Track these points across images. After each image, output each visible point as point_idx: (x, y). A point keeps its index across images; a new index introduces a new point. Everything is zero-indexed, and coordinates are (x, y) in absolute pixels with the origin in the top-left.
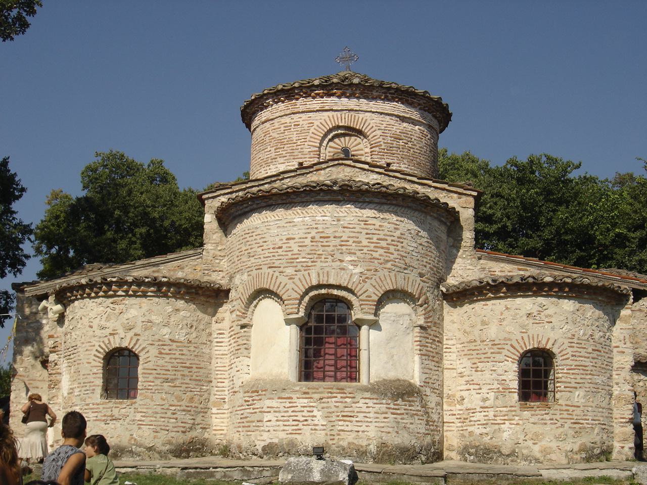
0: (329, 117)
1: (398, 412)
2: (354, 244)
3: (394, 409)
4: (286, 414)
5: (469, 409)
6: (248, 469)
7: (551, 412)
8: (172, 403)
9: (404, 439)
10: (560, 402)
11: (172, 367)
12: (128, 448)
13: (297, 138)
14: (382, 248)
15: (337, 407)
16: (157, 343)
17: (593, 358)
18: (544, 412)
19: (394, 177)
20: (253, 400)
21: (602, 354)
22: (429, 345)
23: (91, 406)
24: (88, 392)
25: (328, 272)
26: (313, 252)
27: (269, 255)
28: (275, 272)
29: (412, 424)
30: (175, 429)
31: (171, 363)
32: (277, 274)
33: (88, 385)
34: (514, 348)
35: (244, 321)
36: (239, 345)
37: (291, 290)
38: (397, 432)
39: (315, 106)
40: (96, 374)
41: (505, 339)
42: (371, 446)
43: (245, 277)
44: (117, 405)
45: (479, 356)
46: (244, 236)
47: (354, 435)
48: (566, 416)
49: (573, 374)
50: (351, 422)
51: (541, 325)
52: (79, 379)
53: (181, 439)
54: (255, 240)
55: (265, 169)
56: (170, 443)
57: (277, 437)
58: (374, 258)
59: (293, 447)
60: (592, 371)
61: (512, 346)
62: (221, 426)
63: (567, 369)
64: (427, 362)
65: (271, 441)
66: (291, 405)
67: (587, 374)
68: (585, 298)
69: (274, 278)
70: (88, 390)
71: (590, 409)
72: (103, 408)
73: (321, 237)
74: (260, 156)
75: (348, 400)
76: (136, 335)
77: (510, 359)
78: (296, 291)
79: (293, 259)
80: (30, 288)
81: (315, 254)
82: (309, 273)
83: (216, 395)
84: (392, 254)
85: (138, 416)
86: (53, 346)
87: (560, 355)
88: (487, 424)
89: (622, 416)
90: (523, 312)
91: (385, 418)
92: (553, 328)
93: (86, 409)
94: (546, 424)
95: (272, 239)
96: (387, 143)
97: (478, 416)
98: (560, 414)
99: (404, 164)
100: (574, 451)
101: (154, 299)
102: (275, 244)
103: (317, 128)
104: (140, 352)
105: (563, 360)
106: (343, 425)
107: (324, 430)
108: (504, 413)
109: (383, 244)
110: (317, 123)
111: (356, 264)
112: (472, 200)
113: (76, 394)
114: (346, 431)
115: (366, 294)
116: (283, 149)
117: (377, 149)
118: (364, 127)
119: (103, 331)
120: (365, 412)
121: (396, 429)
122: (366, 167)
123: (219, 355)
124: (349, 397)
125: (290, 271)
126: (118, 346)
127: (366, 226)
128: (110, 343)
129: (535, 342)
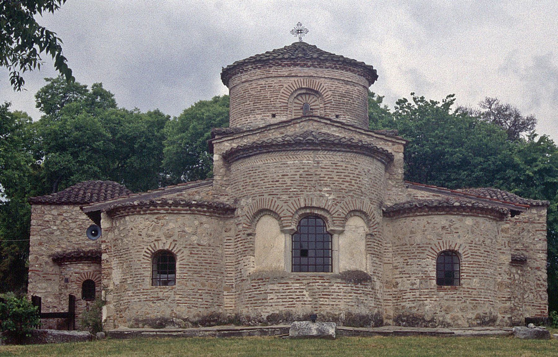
0: (295, 81)
1: (359, 292)
2: (329, 180)
3: (355, 290)
4: (284, 294)
5: (402, 291)
6: (265, 330)
7: (458, 292)
8: (200, 288)
9: (363, 311)
10: (464, 286)
11: (199, 263)
12: (170, 319)
13: (271, 96)
14: (348, 182)
15: (319, 289)
16: (188, 247)
17: (485, 257)
18: (453, 293)
19: (349, 129)
20: (259, 285)
21: (490, 253)
22: (376, 247)
23: (142, 291)
24: (139, 281)
25: (311, 198)
26: (301, 185)
27: (269, 186)
28: (273, 197)
29: (366, 300)
30: (201, 306)
31: (198, 260)
32: (275, 199)
33: (139, 276)
34: (433, 250)
35: (249, 231)
36: (246, 248)
37: (286, 211)
38: (358, 306)
39: (284, 73)
40: (145, 268)
41: (427, 244)
42: (342, 315)
43: (250, 200)
44: (161, 290)
45: (408, 255)
46: (248, 172)
47: (330, 307)
48: (468, 295)
49: (472, 267)
50: (328, 298)
51: (451, 234)
52: (131, 272)
53: (204, 312)
54: (258, 175)
55: (245, 117)
56: (198, 316)
57: (278, 310)
58: (342, 189)
59: (289, 316)
60: (484, 265)
61: (431, 248)
62: (231, 304)
63: (468, 264)
64: (375, 259)
65: (273, 312)
66: (288, 288)
67: (481, 267)
68: (480, 217)
69: (273, 202)
70: (139, 280)
71: (483, 291)
73: (307, 175)
74: (241, 107)
75: (326, 284)
76: (174, 241)
77: (430, 257)
78: (290, 211)
79: (287, 189)
80: (87, 207)
81: (303, 186)
82: (298, 199)
83: (226, 282)
84: (354, 186)
85: (177, 297)
86: (105, 248)
87: (463, 254)
88: (414, 300)
89: (503, 296)
90: (439, 226)
91: (350, 296)
92: (459, 237)
93: (137, 293)
94: (454, 300)
95: (270, 175)
96: (336, 100)
97: (408, 295)
98: (464, 294)
99: (348, 115)
100: (473, 318)
101: (186, 215)
102: (273, 179)
103: (286, 89)
104: (177, 253)
105: (466, 258)
106: (323, 301)
107: (310, 304)
108: (426, 293)
109: (348, 179)
111: (330, 193)
112: (402, 147)
113: (128, 282)
114: (325, 305)
115: (337, 213)
117: (329, 105)
118: (320, 89)
119: (150, 238)
120: (338, 292)
121: (357, 304)
122: (329, 122)
123: (228, 254)
124: (327, 282)
125: (285, 197)
126: (161, 248)
127: (337, 167)
128: (155, 246)
129: (448, 246)
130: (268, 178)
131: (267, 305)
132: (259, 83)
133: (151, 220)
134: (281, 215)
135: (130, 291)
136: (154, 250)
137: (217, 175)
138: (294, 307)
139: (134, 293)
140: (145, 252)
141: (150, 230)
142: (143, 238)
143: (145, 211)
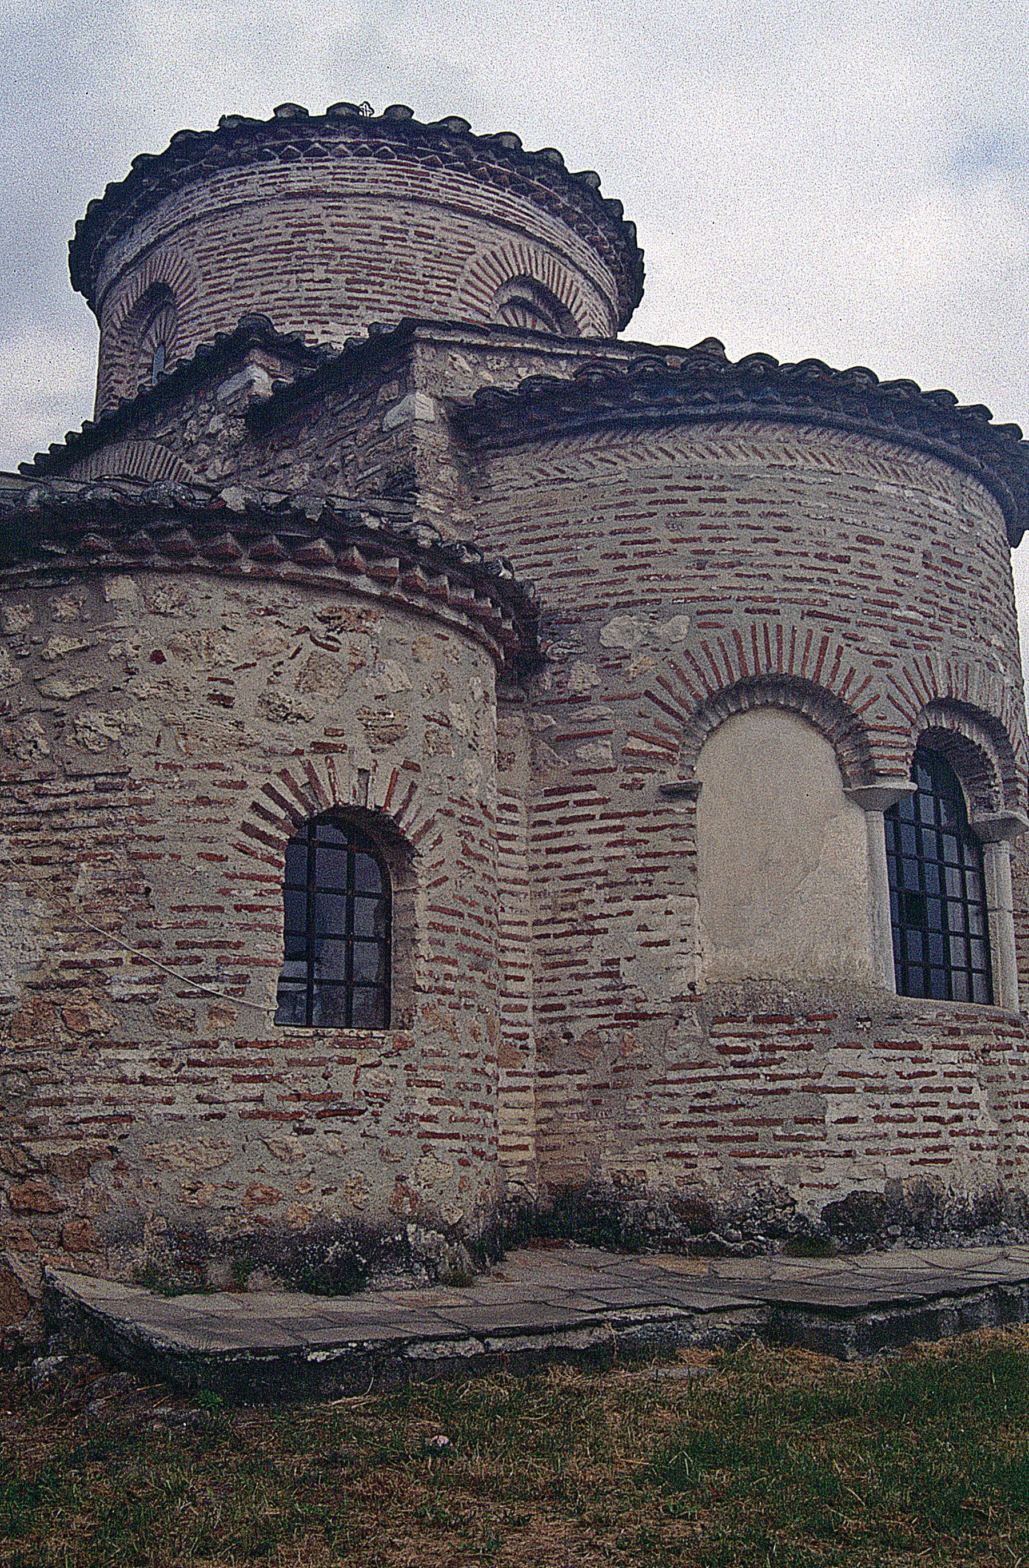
4: (905, 1099)
20: (773, 1048)
23: (227, 1050)
33: (213, 954)
35: (672, 777)
37: (883, 699)
40: (251, 908)
59: (930, 1205)
70: (208, 979)
72: (290, 1063)
85: (422, 1100)
95: (807, 524)
102: (823, 544)
110: (482, 250)
116: (377, 288)
119: (284, 729)
125: (877, 639)
126: (347, 799)
128: (313, 782)
130: (795, 536)
131: (823, 1153)
132: (378, 210)
133: (293, 618)
134: (868, 718)
135: (134, 1045)
136: (310, 808)
137: (427, 488)
138: (946, 1161)
139: (165, 1063)
140: (256, 807)
141: (289, 679)
142: (239, 724)
143: (272, 558)
